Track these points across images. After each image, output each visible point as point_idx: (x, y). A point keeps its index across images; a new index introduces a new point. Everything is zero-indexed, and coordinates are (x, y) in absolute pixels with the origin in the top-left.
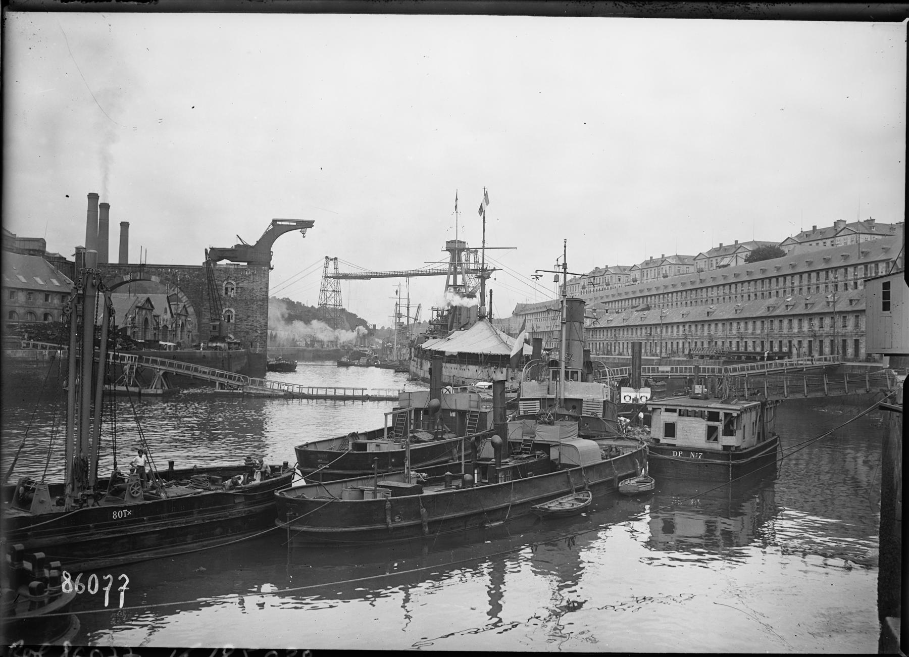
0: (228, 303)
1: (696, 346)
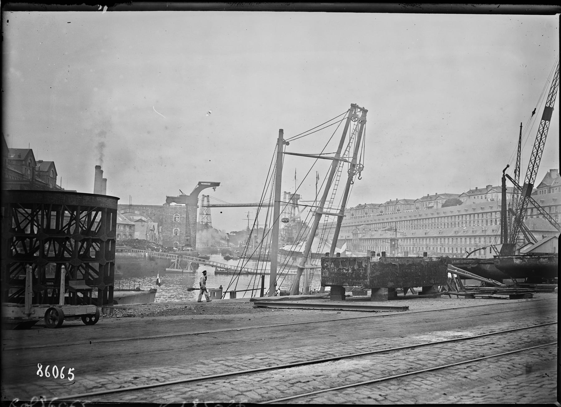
0: (176, 225)
1: (419, 249)
